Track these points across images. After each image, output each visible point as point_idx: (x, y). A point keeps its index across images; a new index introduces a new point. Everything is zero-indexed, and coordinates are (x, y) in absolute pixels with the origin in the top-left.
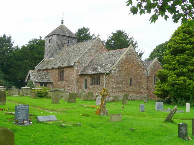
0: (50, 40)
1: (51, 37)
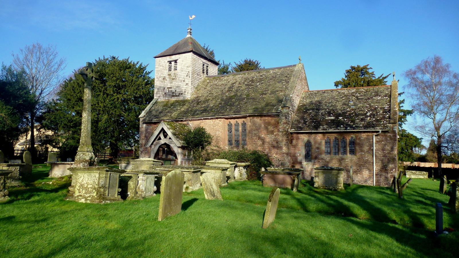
0: (170, 62)
1: (174, 57)
